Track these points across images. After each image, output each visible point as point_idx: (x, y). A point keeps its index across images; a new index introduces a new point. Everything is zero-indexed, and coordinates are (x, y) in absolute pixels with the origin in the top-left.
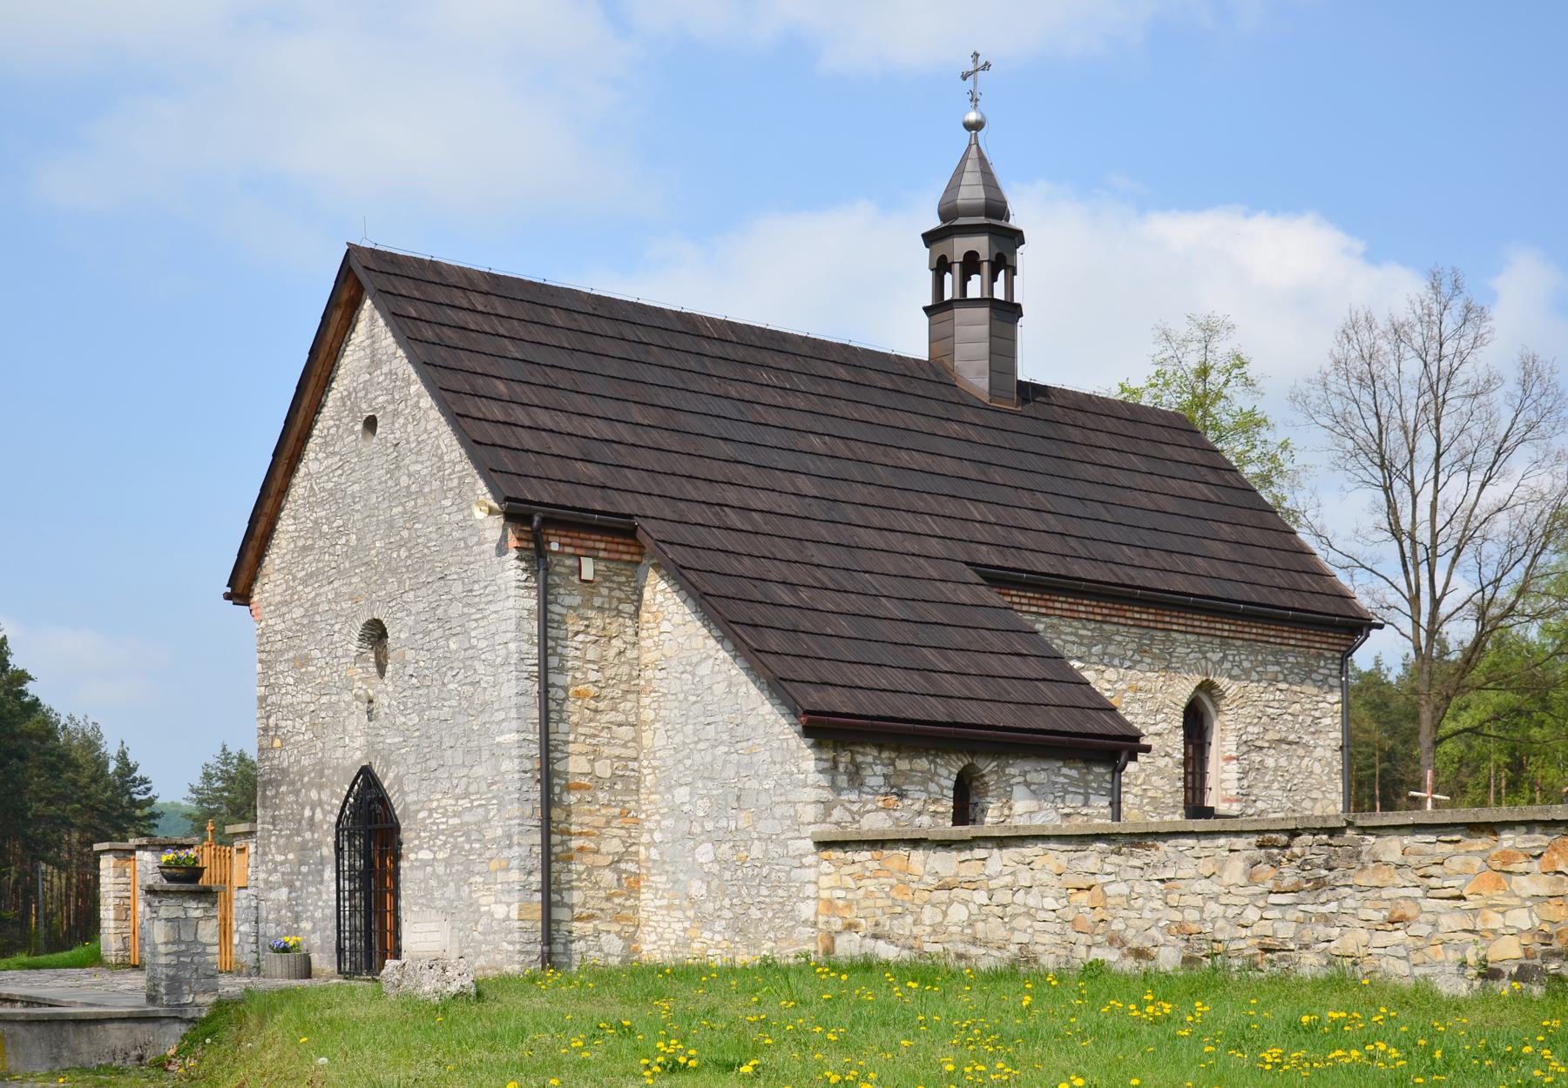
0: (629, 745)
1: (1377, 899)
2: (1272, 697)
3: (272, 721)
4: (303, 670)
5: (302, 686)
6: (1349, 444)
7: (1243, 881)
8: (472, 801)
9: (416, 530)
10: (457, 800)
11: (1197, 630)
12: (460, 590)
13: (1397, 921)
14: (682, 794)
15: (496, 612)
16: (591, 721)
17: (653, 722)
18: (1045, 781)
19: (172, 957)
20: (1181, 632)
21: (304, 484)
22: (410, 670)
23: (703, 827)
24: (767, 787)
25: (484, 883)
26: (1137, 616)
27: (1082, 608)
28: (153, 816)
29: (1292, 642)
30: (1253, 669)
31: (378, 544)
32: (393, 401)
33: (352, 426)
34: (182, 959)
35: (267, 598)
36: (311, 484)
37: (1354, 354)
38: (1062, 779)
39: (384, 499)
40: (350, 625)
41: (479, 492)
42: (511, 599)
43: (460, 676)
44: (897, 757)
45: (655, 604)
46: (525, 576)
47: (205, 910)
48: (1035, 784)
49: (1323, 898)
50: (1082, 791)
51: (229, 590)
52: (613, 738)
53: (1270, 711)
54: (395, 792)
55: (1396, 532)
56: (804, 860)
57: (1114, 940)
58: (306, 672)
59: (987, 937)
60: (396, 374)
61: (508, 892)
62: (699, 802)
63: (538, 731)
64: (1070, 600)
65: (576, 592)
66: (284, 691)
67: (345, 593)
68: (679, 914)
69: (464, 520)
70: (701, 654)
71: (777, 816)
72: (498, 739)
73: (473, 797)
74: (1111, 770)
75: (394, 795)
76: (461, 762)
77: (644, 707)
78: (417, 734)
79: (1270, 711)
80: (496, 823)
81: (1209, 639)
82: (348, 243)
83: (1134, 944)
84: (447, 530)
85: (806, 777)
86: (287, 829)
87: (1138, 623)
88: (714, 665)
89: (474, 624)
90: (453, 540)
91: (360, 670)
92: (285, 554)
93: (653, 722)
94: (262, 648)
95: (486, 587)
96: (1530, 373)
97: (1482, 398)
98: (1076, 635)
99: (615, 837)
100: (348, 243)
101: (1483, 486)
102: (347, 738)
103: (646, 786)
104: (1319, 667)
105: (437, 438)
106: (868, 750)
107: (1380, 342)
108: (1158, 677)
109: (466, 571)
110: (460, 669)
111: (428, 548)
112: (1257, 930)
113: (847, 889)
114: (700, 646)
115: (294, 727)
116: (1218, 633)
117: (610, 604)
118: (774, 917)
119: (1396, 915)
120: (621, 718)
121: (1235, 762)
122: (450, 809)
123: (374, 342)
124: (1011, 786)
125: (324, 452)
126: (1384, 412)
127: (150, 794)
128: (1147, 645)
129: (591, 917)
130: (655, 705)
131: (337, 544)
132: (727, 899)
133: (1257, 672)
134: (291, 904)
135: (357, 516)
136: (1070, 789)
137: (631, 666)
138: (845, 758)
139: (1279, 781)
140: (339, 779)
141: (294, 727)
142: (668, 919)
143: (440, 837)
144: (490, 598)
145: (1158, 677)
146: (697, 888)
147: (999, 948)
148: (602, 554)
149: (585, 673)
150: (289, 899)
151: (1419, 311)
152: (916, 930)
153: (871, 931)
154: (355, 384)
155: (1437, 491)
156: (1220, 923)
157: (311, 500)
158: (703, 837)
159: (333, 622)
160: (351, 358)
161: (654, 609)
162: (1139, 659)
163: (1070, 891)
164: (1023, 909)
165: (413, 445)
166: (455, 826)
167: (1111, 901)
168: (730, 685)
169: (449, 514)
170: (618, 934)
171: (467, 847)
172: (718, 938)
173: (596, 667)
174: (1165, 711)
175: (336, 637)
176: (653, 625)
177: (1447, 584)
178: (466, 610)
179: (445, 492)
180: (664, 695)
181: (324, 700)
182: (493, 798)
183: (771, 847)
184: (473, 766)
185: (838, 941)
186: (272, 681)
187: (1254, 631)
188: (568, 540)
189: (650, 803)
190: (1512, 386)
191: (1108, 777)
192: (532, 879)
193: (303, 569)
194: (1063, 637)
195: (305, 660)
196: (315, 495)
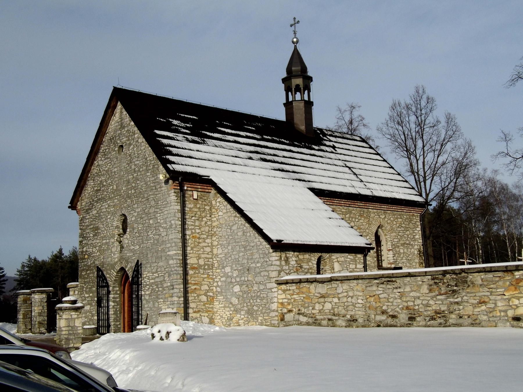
0: (209, 253)
1: (474, 296)
2: (400, 229)
3: (84, 249)
4: (96, 232)
5: (96, 237)
6: (397, 144)
7: (427, 291)
8: (158, 274)
9: (138, 184)
10: (153, 274)
11: (377, 208)
12: (154, 203)
13: (482, 302)
14: (228, 269)
15: (167, 211)
16: (197, 246)
17: (217, 245)
18: (344, 260)
19: (67, 332)
20: (372, 209)
21: (97, 169)
22: (136, 231)
23: (236, 280)
24: (258, 266)
25: (163, 302)
26: (359, 204)
27: (343, 202)
28: (4, 281)
29: (405, 211)
30: (394, 220)
31: (124, 188)
32: (129, 140)
33: (114, 149)
34: (70, 332)
35: (83, 208)
36: (100, 169)
37: (395, 115)
38: (348, 260)
39: (126, 173)
40: (114, 216)
41: (160, 170)
42: (172, 206)
43: (154, 232)
44: (299, 254)
45: (216, 206)
46: (176, 198)
47: (78, 315)
48: (340, 261)
49: (456, 297)
50: (354, 263)
51: (70, 205)
52: (204, 251)
53: (400, 234)
54: (130, 272)
55: (413, 172)
56: (272, 290)
57: (383, 312)
58: (98, 232)
59: (339, 313)
60: (130, 131)
61: (173, 304)
62: (234, 272)
63: (181, 250)
64: (339, 200)
65: (192, 203)
66: (89, 239)
67: (112, 205)
68: (228, 309)
69: (155, 180)
70: (233, 222)
71: (262, 275)
72: (168, 253)
73: (159, 273)
74: (363, 256)
75: (129, 273)
76: (154, 261)
77: (214, 241)
78: (138, 252)
79: (400, 234)
80: (168, 281)
81: (380, 211)
82: (114, 87)
83: (391, 314)
84: (149, 183)
85: (272, 262)
86: (90, 286)
87: (359, 206)
88: (238, 226)
89: (159, 215)
90: (151, 187)
91: (117, 231)
92: (90, 193)
93: (217, 245)
94: (81, 225)
95: (163, 202)
96: (449, 119)
97: (435, 127)
98: (341, 211)
99: (205, 284)
100: (114, 87)
101: (438, 157)
102: (112, 254)
103: (215, 267)
104: (413, 219)
105: (145, 152)
106: (290, 253)
107: (402, 111)
108: (366, 224)
109: (155, 197)
110: (154, 230)
111: (142, 189)
112: (434, 308)
113: (289, 299)
114: (233, 219)
115: (93, 251)
116: (383, 209)
117: (202, 206)
118: (262, 309)
119: (482, 301)
120: (206, 244)
121: (391, 251)
122: (150, 277)
123: (122, 120)
124: (334, 262)
125: (104, 157)
126: (406, 133)
127: (3, 273)
128: (362, 214)
129: (199, 311)
130: (217, 240)
131: (109, 189)
132: (245, 304)
133: (395, 221)
134: (91, 311)
135: (116, 179)
136: (351, 263)
137: (209, 227)
138: (283, 255)
139: (405, 257)
140: (109, 268)
141: (93, 251)
142: (224, 311)
143: (147, 287)
144: (165, 206)
145: (366, 224)
146: (235, 301)
147: (343, 316)
148: (199, 190)
149: (195, 230)
150: (90, 309)
151: (413, 99)
152: (314, 311)
153: (297, 312)
154: (115, 134)
155: (424, 158)
156: (421, 306)
157: (99, 174)
158: (236, 283)
159: (107, 215)
160: (114, 126)
161: (216, 208)
162: (360, 218)
163: (367, 297)
164: (351, 304)
165: (136, 155)
166: (152, 283)
167: (381, 300)
168: (244, 233)
169: (149, 178)
170: (207, 316)
171: (157, 289)
172: (242, 317)
173: (199, 228)
174: (369, 235)
175: (108, 220)
176: (216, 213)
177: (430, 188)
178: (156, 210)
179: (148, 170)
180: (221, 236)
181: (104, 241)
182: (166, 273)
183: (260, 285)
184: (159, 263)
185: (285, 316)
186: (85, 235)
187: (394, 208)
188: (189, 186)
189: (216, 273)
190: (443, 123)
191: (362, 258)
192: (180, 299)
193: (96, 198)
194: (337, 212)
195: (97, 228)
196: (101, 172)
